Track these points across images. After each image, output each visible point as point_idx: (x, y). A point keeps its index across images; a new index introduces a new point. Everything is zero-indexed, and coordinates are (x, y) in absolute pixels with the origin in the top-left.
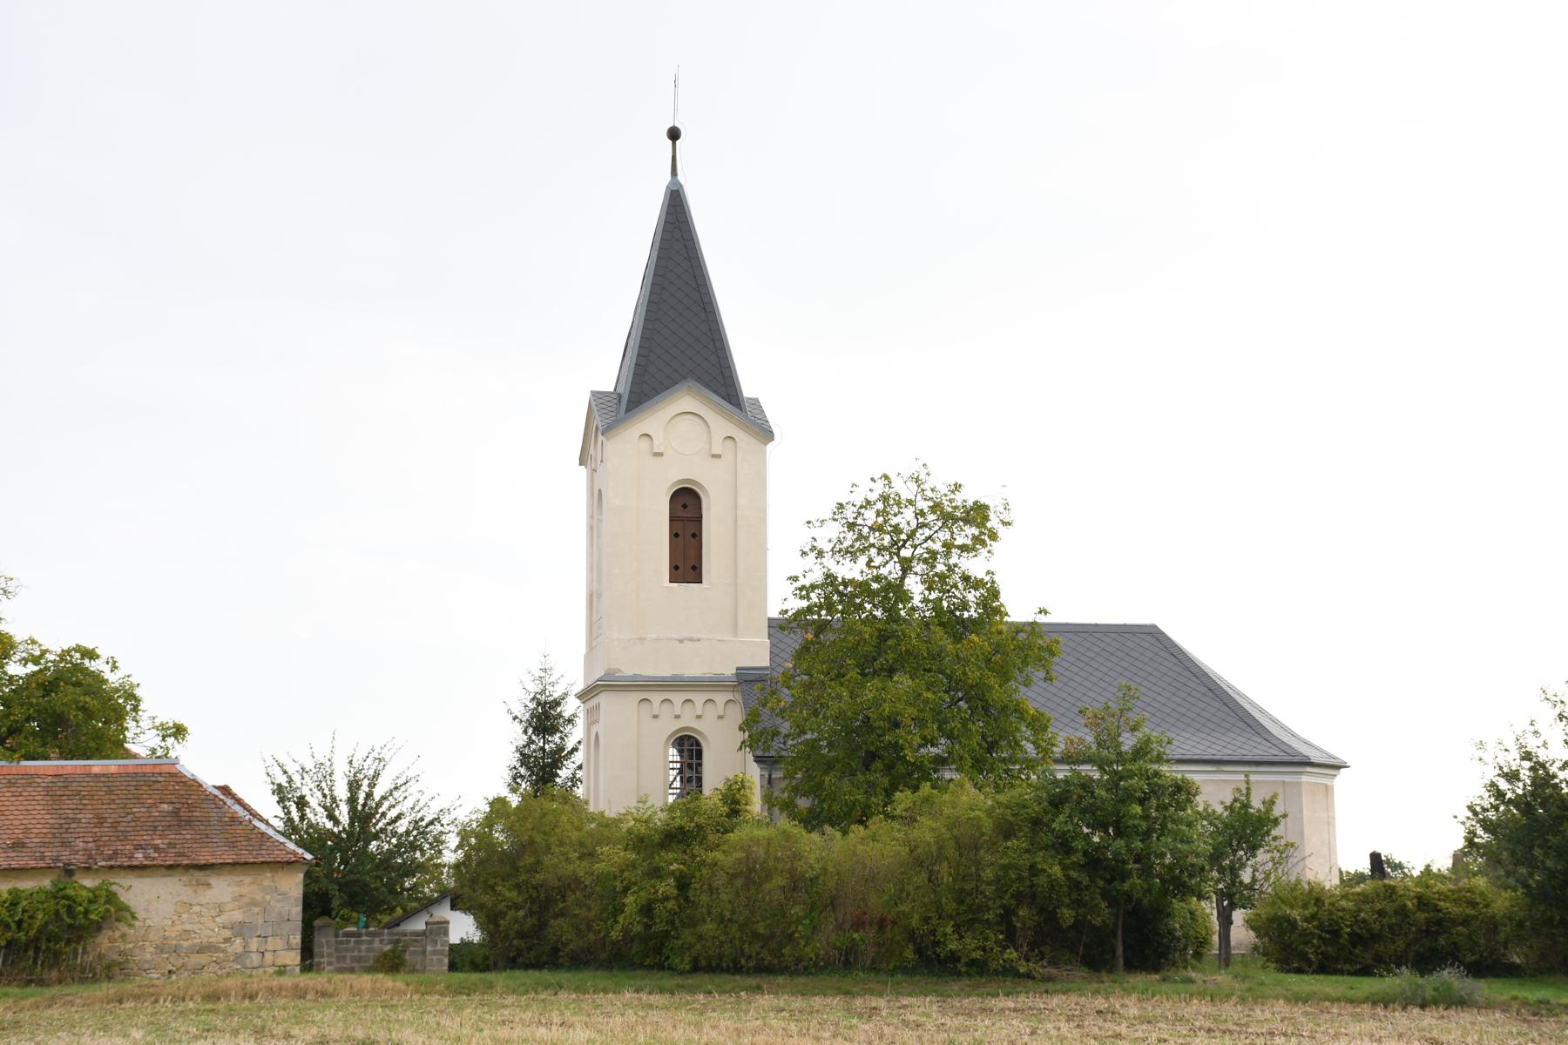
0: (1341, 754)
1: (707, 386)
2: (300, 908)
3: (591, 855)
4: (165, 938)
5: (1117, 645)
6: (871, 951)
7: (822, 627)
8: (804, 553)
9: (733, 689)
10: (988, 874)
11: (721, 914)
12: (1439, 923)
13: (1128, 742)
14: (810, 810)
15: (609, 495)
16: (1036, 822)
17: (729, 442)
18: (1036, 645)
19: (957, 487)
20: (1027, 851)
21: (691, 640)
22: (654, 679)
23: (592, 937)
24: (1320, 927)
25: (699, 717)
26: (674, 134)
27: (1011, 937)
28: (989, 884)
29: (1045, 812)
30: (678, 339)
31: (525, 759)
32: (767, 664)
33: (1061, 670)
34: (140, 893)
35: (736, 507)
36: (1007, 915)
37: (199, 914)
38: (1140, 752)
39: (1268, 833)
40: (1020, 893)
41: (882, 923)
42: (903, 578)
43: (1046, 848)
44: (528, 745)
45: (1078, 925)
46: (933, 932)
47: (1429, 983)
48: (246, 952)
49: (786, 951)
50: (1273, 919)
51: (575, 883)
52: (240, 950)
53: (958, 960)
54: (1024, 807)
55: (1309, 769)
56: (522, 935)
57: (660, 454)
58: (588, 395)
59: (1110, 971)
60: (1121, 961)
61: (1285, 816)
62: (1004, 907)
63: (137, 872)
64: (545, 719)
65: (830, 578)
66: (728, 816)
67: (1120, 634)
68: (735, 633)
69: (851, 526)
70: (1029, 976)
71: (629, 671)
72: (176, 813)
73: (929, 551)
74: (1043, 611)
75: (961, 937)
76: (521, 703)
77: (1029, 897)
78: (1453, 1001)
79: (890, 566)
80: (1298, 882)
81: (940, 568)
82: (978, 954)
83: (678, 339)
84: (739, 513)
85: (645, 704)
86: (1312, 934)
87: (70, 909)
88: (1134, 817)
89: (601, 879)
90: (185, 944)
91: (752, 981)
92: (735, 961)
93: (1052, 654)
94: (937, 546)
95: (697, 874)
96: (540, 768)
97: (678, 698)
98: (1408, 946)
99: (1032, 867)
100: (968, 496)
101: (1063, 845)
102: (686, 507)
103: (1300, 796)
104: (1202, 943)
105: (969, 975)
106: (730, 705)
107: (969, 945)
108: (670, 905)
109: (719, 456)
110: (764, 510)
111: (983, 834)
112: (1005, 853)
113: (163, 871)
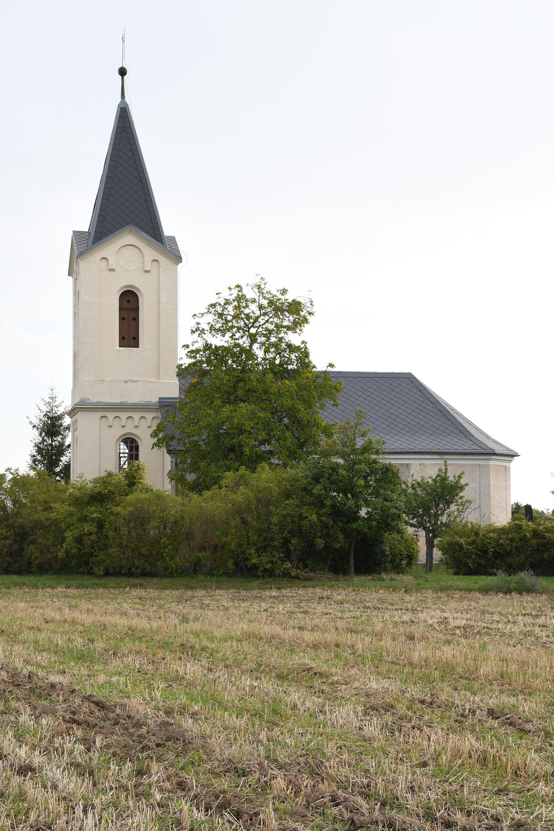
0: (515, 448)
1: (142, 229)
3: (48, 509)
5: (388, 385)
6: (209, 564)
7: (205, 373)
8: (193, 332)
9: (156, 410)
10: (275, 519)
11: (121, 543)
12: (545, 545)
13: (360, 443)
14: (194, 481)
15: (82, 294)
16: (305, 489)
17: (155, 263)
18: (331, 384)
19: (284, 292)
20: (298, 506)
21: (132, 381)
22: (109, 404)
23: (49, 556)
24: (477, 548)
25: (136, 427)
26: (123, 72)
27: (288, 556)
28: (276, 525)
29: (310, 484)
30: (126, 200)
31: (40, 450)
33: (341, 402)
35: (159, 303)
36: (287, 541)
38: (366, 449)
39: (457, 495)
40: (292, 530)
41: (216, 547)
42: (251, 346)
43: (309, 504)
44: (43, 442)
45: (327, 548)
46: (244, 553)
47: (514, 579)
49: (159, 563)
50: (450, 544)
51: (38, 525)
53: (257, 568)
54: (298, 481)
55: (494, 457)
56: (11, 555)
57: (113, 270)
58: (72, 233)
59: (345, 574)
60: (353, 569)
61: (467, 485)
62: (285, 538)
64: (51, 427)
65: (207, 347)
66: (128, 485)
67: (389, 378)
68: (158, 376)
69: (221, 315)
70: (297, 577)
71: (94, 399)
73: (267, 329)
74: (331, 365)
75: (259, 556)
76: (37, 416)
77: (299, 532)
78: (523, 589)
79: (245, 338)
80: (466, 523)
81: (273, 339)
82: (269, 566)
83: (126, 200)
84: (161, 306)
85: (104, 419)
86: (472, 552)
88: (359, 487)
89: (56, 523)
91: (137, 581)
92: (130, 570)
93: (337, 391)
94: (271, 327)
95: (108, 520)
96: (50, 455)
97: (124, 416)
98: (527, 558)
99: (300, 515)
100: (290, 297)
101: (319, 503)
102: (129, 301)
103: (489, 472)
104: (411, 558)
105: (263, 576)
108: (93, 537)
109: (149, 272)
111: (272, 497)
112: (285, 508)
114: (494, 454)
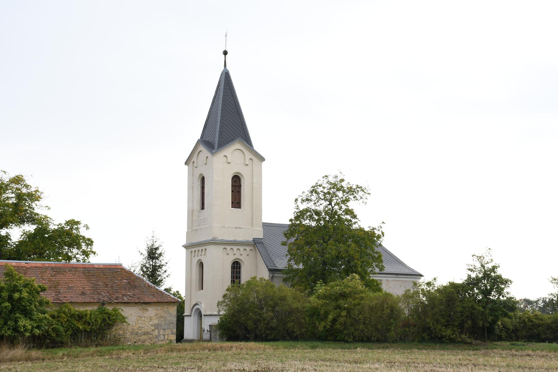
2: (176, 319)
4: (133, 329)
17: (251, 160)
19: (342, 180)
21: (239, 228)
26: (225, 53)
30: (226, 123)
32: (262, 237)
34: (131, 314)
35: (253, 183)
37: (144, 321)
48: (159, 335)
52: (157, 334)
57: (229, 163)
63: (126, 305)
71: (220, 238)
72: (129, 283)
83: (226, 123)
87: (109, 318)
90: (140, 332)
97: (235, 248)
102: (236, 181)
106: (251, 251)
107: (448, 332)
110: (261, 184)
113: (133, 305)
114: (191, 279)
